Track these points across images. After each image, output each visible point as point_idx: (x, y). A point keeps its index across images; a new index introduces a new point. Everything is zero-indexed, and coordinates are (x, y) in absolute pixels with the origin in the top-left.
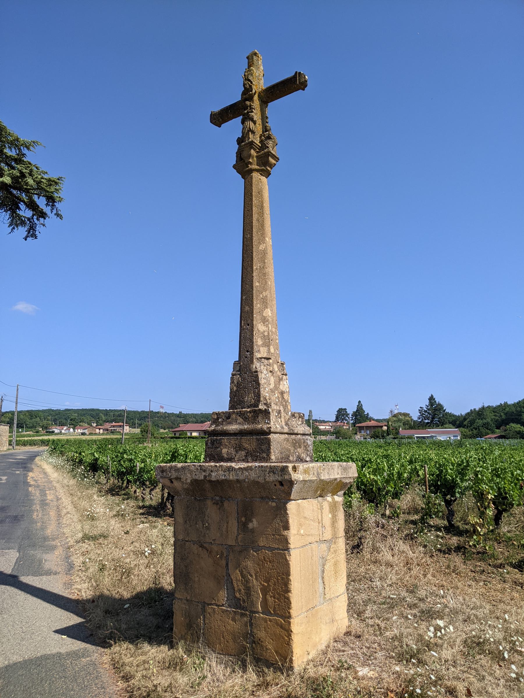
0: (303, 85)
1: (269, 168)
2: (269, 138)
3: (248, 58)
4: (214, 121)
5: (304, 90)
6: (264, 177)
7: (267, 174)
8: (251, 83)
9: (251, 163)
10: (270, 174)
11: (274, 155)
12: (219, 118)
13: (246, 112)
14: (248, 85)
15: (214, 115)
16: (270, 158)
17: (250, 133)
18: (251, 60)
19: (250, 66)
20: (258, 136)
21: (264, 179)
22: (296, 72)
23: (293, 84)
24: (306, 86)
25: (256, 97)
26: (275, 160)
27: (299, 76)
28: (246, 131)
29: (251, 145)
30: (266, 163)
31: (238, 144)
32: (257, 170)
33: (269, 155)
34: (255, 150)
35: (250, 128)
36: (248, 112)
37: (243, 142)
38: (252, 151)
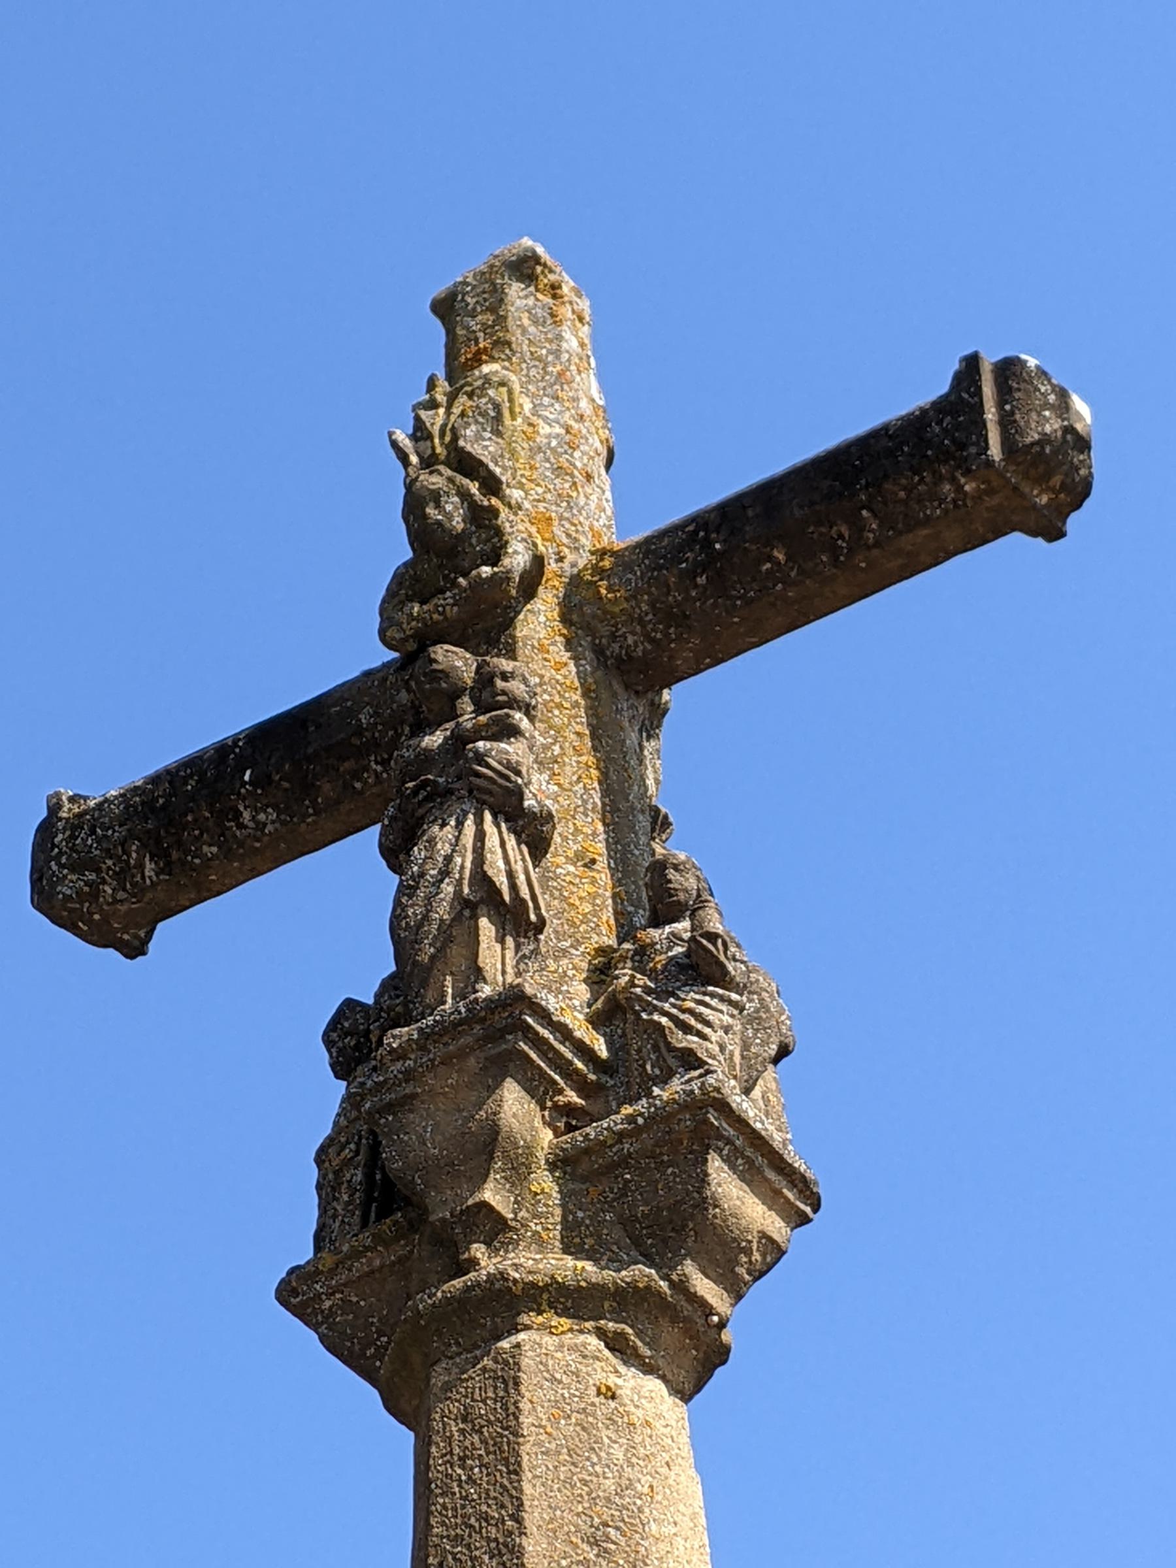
0: (1045, 486)
1: (705, 1287)
2: (702, 967)
3: (446, 308)
4: (70, 884)
5: (1054, 533)
6: (654, 1385)
7: (694, 1356)
8: (492, 485)
9: (495, 1229)
10: (721, 1354)
11: (758, 1141)
12: (132, 863)
13: (434, 740)
14: (452, 504)
15: (76, 824)
16: (717, 1168)
17: (486, 927)
18: (468, 324)
19: (460, 365)
20: (576, 964)
21: (647, 1395)
22: (972, 363)
23: (946, 477)
24: (1078, 492)
25: (539, 621)
26: (772, 1199)
27: (1004, 392)
28: (443, 911)
29: (498, 1035)
30: (665, 1213)
31: (342, 1069)
32: (573, 1302)
33: (703, 1140)
34: (539, 1089)
35: (481, 878)
36: (459, 741)
37: (407, 1053)
38: (514, 1104)
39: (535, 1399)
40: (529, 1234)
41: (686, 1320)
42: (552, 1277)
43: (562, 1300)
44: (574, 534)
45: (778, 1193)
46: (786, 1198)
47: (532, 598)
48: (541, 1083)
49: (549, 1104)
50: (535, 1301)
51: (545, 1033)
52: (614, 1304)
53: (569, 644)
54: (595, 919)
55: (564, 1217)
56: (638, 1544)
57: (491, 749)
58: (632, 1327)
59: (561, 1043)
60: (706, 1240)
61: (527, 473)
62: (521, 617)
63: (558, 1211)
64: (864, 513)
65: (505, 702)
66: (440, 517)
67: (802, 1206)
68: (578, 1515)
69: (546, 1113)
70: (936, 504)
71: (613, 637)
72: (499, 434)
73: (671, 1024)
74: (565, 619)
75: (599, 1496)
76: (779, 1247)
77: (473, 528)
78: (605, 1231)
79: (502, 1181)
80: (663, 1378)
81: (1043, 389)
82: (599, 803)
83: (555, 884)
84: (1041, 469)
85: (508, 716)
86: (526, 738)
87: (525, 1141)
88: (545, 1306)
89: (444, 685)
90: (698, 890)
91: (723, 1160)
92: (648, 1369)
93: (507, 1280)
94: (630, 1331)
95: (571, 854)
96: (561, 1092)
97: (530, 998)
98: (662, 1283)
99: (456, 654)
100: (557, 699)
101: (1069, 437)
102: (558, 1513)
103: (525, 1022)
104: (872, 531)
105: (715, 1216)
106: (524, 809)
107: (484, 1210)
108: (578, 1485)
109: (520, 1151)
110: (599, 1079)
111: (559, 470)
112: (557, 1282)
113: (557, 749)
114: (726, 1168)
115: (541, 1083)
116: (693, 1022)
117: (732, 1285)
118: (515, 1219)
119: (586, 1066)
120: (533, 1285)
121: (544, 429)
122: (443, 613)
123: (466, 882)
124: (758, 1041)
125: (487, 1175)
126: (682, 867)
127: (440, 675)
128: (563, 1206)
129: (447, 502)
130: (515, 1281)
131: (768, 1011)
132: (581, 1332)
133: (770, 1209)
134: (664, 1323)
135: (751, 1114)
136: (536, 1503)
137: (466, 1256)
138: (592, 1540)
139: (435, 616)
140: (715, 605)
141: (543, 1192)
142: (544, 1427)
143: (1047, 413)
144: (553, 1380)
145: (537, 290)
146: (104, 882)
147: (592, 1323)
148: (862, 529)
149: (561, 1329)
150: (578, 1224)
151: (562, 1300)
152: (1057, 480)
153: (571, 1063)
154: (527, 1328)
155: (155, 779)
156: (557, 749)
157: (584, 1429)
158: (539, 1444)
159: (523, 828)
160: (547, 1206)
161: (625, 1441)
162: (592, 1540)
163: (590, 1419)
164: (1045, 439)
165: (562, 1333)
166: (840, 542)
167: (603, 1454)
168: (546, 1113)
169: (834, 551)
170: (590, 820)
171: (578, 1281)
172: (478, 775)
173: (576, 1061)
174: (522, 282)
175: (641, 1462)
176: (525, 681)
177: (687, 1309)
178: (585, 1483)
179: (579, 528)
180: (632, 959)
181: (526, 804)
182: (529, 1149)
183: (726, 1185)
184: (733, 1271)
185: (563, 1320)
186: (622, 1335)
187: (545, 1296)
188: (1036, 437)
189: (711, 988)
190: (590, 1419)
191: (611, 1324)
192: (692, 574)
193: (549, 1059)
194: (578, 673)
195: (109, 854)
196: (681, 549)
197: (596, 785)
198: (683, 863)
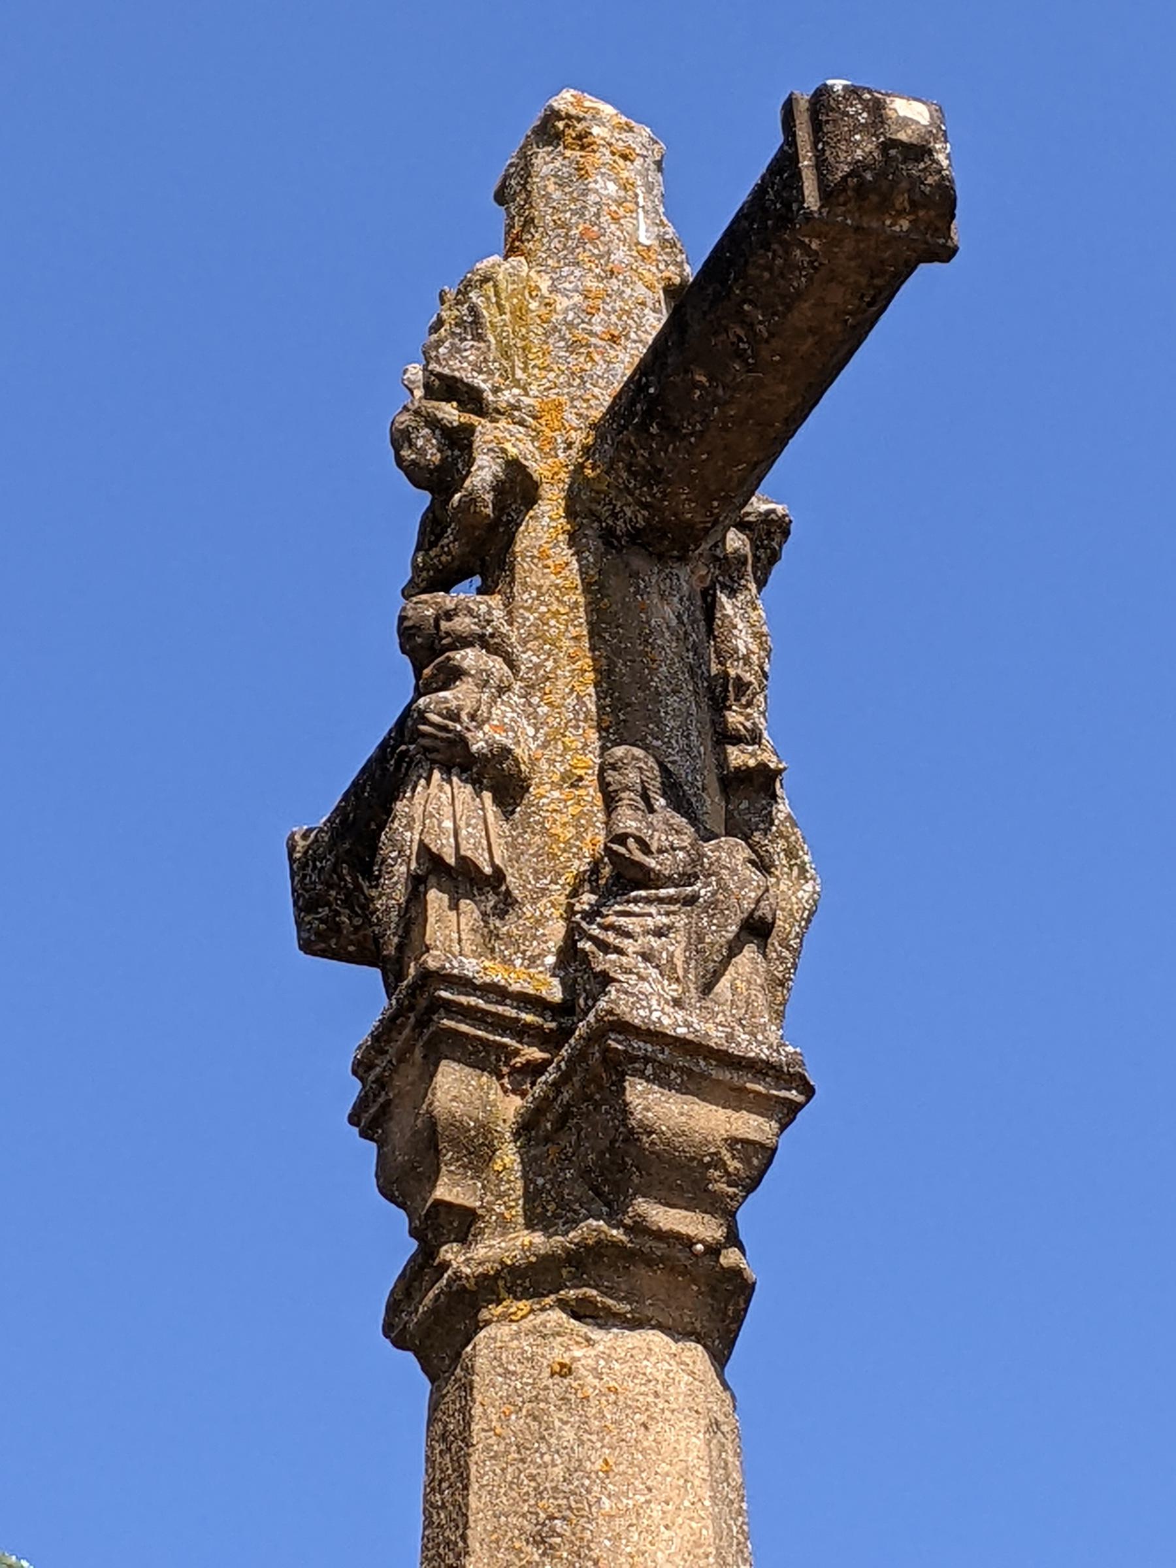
24: (942, 202)
26: (737, 1099)
27: (817, 127)
29: (423, 1023)
32: (528, 1280)
33: (618, 1068)
34: (482, 1058)
39: (487, 1401)
40: (494, 1218)
41: (662, 1259)
42: (502, 1262)
43: (519, 1282)
44: (585, 412)
45: (743, 1090)
46: (758, 1093)
47: (535, 502)
48: (488, 1053)
49: (505, 1070)
50: (493, 1292)
51: (473, 1001)
52: (573, 1269)
53: (573, 539)
54: (578, 843)
55: (526, 1188)
56: (584, 1529)
57: (430, 703)
58: (595, 1287)
59: (497, 1003)
60: (652, 1171)
61: (538, 362)
62: (522, 528)
63: (519, 1185)
64: (746, 307)
65: (450, 644)
66: (413, 456)
67: (783, 1094)
68: (524, 1516)
69: (506, 1080)
70: (797, 273)
71: (614, 515)
72: (479, 338)
73: (594, 949)
74: (570, 513)
75: (546, 1489)
76: (762, 1146)
77: (457, 453)
78: (567, 1191)
79: (461, 1170)
80: (660, 1327)
81: (851, 111)
82: (594, 709)
83: (537, 818)
85: (449, 659)
86: (472, 676)
87: (477, 1120)
88: (504, 1294)
89: (419, 640)
90: (642, 782)
91: (648, 1080)
92: (635, 1324)
93: (460, 1278)
94: (595, 1293)
95: (556, 778)
96: (516, 1053)
97: (437, 972)
98: (614, 1232)
99: (426, 602)
100: (554, 608)
101: (893, 152)
102: (503, 1519)
103: (440, 997)
104: (760, 323)
105: (653, 1143)
106: (473, 755)
107: (442, 1209)
108: (526, 1482)
109: (473, 1133)
110: (560, 1024)
111: (573, 347)
112: (507, 1266)
113: (550, 664)
114: (656, 1088)
115: (488, 1053)
116: (672, 908)
117: (712, 1204)
118: (482, 1207)
119: (542, 1016)
120: (485, 1276)
121: (562, 303)
122: (449, 553)
123: (414, 857)
124: (714, 928)
125: (438, 1170)
126: (620, 764)
127: (412, 632)
128: (525, 1176)
129: (418, 437)
130: (467, 1277)
131: (726, 889)
132: (543, 1309)
133: (737, 1109)
134: (642, 1271)
135: (666, 1021)
136: (481, 1515)
137: (437, 1261)
138: (538, 1538)
139: (444, 558)
140: (676, 450)
141: (505, 1168)
142: (493, 1429)
143: (858, 137)
144: (507, 1373)
145: (565, 147)
146: (338, 914)
147: (553, 1297)
148: (752, 325)
149: (520, 1313)
150: (539, 1191)
151: (519, 1282)
152: (901, 201)
153: (517, 1020)
154: (488, 1323)
155: (346, 797)
156: (550, 664)
157: (535, 1419)
158: (488, 1448)
159: (481, 775)
160: (509, 1181)
161: (578, 1418)
162: (538, 1538)
163: (542, 1405)
164: (858, 169)
165: (523, 1317)
166: (741, 346)
167: (553, 1441)
168: (506, 1080)
169: (740, 355)
170: (581, 731)
171: (528, 1257)
172: (424, 735)
173: (523, 1015)
174: (550, 144)
175: (594, 1438)
176: (470, 612)
177: (660, 1248)
178: (532, 1478)
179: (593, 402)
180: (590, 881)
181: (474, 748)
182: (485, 1129)
183: (655, 1105)
184: (706, 1190)
185: (521, 1304)
186: (584, 1301)
187: (501, 1283)
188: (846, 169)
189: (633, 894)
190: (542, 1405)
191: (572, 1292)
192: (643, 427)
193: (491, 1024)
194: (580, 570)
195: (330, 886)
196: (633, 403)
197: (591, 690)
198: (621, 759)
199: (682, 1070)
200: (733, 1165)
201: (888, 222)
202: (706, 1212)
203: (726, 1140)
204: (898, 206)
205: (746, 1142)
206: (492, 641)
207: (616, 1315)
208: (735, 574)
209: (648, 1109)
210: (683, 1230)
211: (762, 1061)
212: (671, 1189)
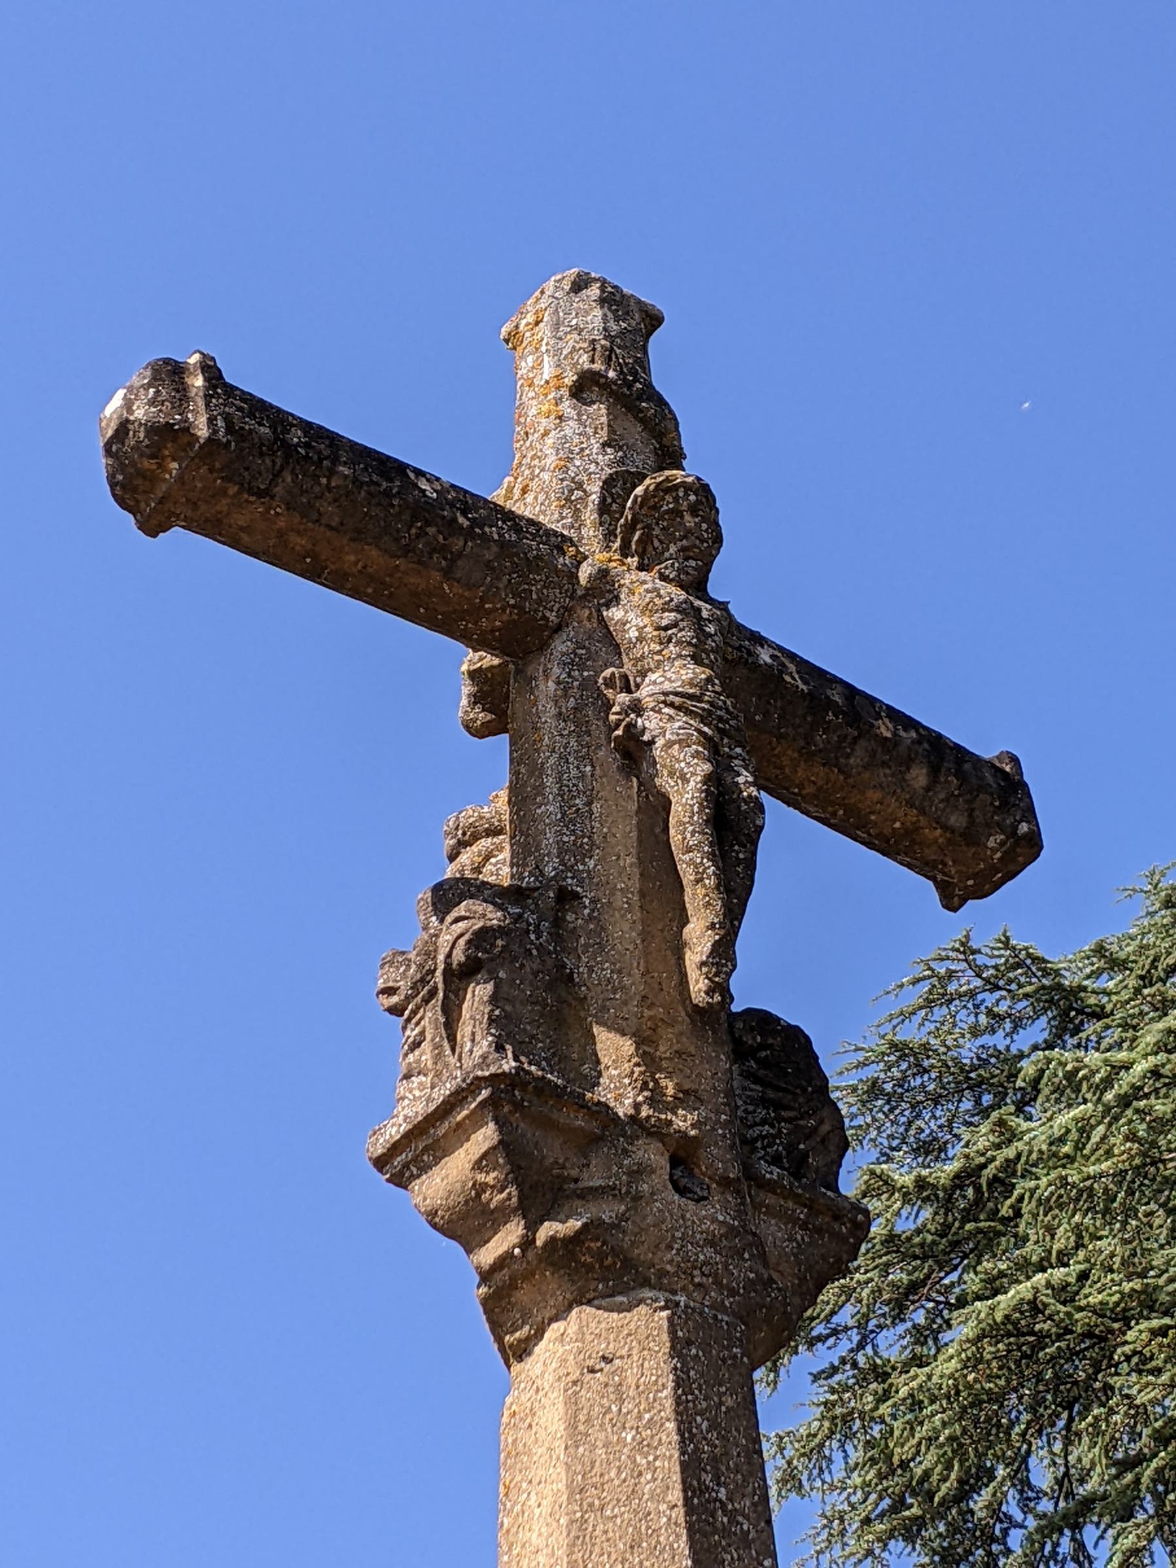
23: (246, 474)
45: (459, 1124)
46: (467, 1117)
84: (138, 481)
92: (539, 1334)
105: (442, 1218)
116: (418, 1016)
184: (493, 1212)
199: (426, 1149)
200: (491, 1178)
201: (167, 476)
202: (505, 1224)
203: (473, 1168)
204: (155, 467)
205: (484, 1156)
206: (467, 837)
207: (528, 1339)
208: (608, 587)
209: (425, 1199)
210: (500, 1251)
211: (449, 1096)
212: (478, 1231)
